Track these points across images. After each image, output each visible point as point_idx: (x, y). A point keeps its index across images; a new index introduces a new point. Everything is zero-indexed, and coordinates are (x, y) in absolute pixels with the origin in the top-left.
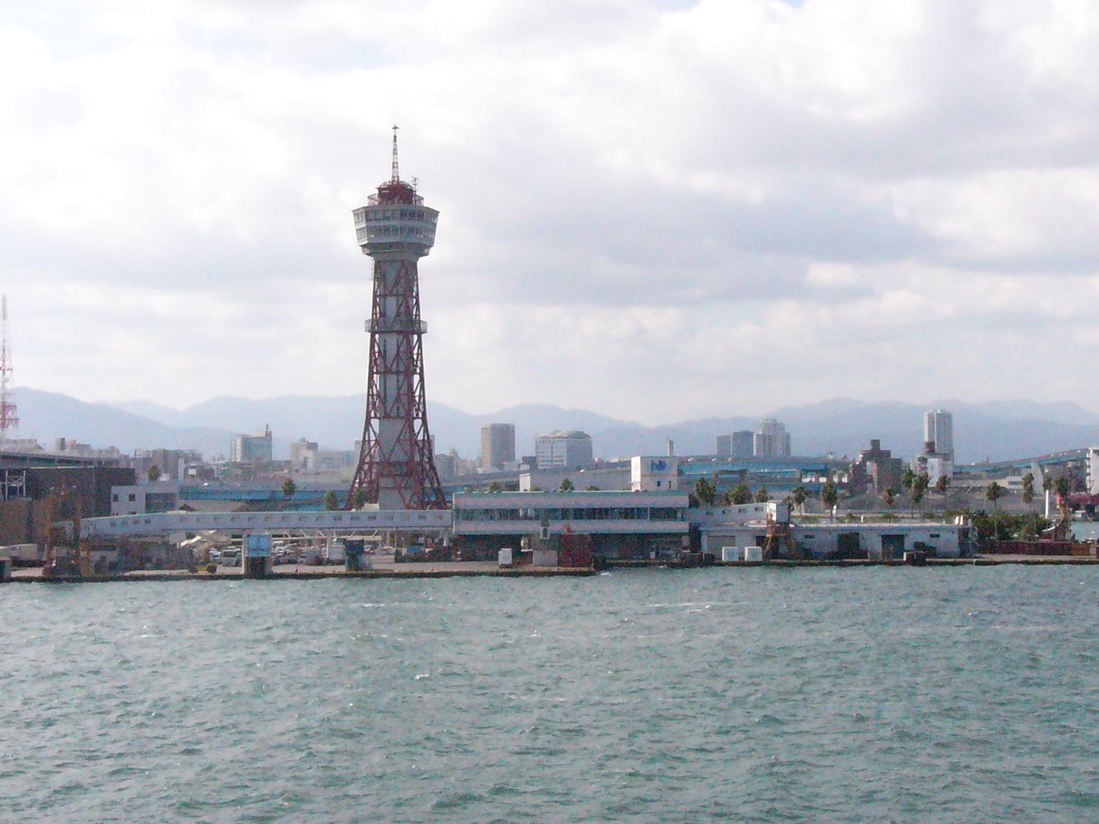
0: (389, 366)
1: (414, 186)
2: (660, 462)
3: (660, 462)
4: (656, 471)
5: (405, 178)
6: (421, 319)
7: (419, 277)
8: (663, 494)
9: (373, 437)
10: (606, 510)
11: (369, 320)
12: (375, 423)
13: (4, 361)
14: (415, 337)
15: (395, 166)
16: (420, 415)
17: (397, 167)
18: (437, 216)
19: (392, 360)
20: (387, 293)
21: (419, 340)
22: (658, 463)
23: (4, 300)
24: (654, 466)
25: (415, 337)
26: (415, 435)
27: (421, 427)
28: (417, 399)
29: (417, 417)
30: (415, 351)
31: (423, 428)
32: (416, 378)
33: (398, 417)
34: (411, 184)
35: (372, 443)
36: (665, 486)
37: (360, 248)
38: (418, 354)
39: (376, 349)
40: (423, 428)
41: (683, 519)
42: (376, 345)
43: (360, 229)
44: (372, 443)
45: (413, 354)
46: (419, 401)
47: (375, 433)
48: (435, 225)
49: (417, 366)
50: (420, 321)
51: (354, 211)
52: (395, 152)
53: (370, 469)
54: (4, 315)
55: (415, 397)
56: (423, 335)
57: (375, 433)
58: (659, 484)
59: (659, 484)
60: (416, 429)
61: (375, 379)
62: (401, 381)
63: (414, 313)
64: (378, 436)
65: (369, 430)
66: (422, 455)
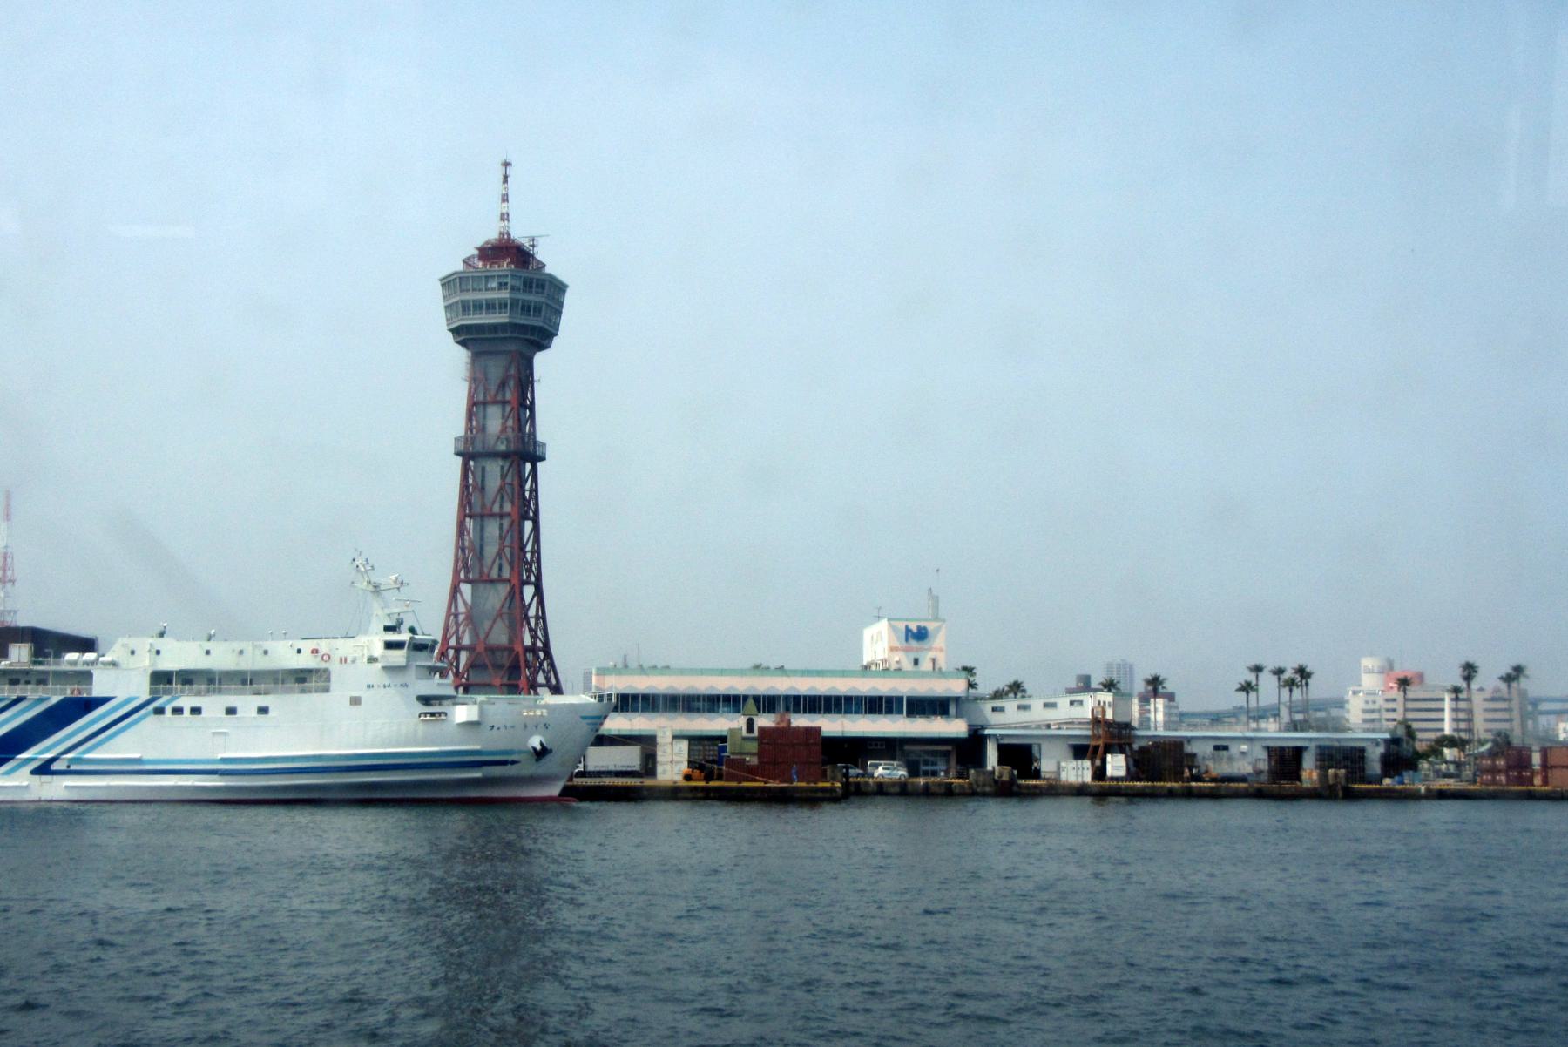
0: (488, 504)
1: (531, 248)
2: (919, 628)
3: (919, 628)
4: (914, 644)
5: (519, 234)
6: (538, 439)
7: (535, 378)
8: (924, 675)
9: (462, 609)
10: (838, 699)
11: (461, 437)
12: (466, 589)
13: (4, 571)
14: (528, 466)
15: (504, 217)
16: (533, 579)
17: (508, 220)
18: (564, 291)
19: (493, 495)
20: (488, 398)
21: (534, 470)
22: (915, 630)
23: (8, 496)
24: (910, 634)
25: (528, 466)
26: (524, 606)
27: (533, 597)
28: (527, 494)
29: (528, 583)
30: (528, 486)
31: (535, 599)
32: (528, 525)
33: (501, 580)
34: (527, 245)
35: (461, 617)
36: (926, 665)
37: (450, 334)
38: (532, 552)
39: (471, 481)
40: (535, 599)
41: (958, 716)
42: (470, 474)
43: (451, 305)
44: (461, 617)
45: (525, 553)
46: (532, 558)
47: (465, 602)
48: (561, 305)
49: (529, 507)
50: (535, 442)
51: (441, 280)
52: (506, 178)
53: (457, 658)
54: (7, 515)
55: (526, 552)
56: (540, 465)
57: (465, 602)
58: (916, 662)
59: (916, 662)
60: (527, 599)
61: (467, 525)
62: (506, 469)
63: (527, 431)
64: (471, 608)
65: (456, 600)
66: (534, 637)
